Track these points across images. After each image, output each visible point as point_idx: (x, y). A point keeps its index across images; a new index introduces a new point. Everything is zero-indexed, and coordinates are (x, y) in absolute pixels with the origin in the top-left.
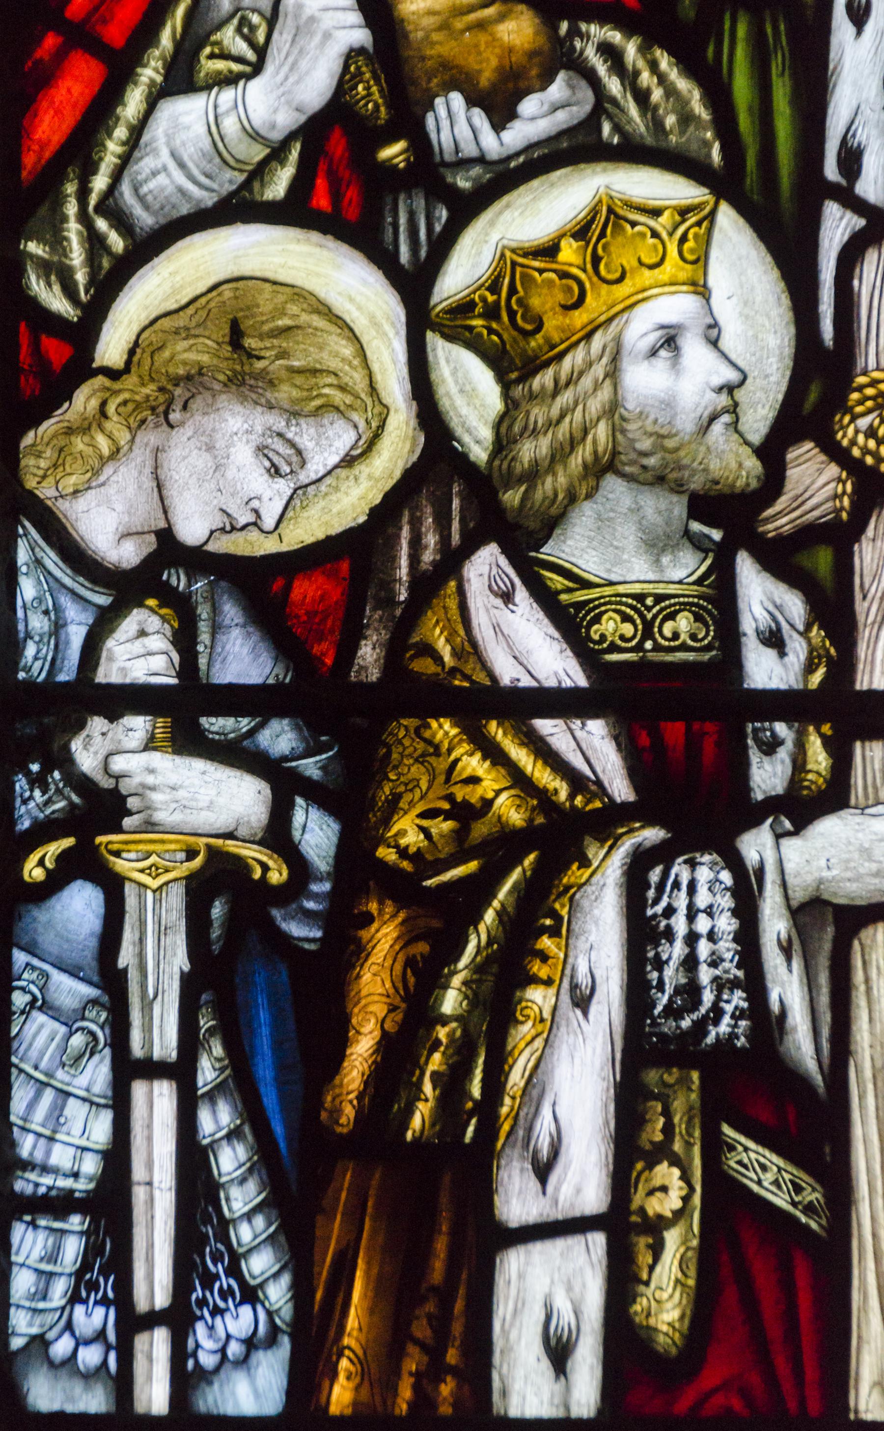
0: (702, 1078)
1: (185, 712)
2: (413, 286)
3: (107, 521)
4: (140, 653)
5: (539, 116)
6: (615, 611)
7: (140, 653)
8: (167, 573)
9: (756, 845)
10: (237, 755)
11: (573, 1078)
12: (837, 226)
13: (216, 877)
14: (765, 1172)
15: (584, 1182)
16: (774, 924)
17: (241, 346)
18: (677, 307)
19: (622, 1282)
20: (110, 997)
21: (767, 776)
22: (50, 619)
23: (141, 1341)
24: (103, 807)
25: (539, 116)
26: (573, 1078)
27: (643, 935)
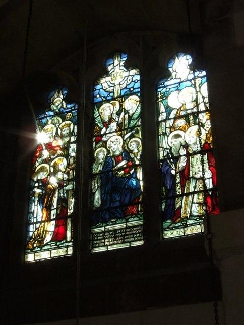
0: (20, 240)
1: (38, 188)
2: (50, 165)
3: (35, 179)
4: (36, 185)
5: (56, 156)
6: (131, 142)
7: (36, 185)
8: (38, 181)
9: (64, 188)
10: (40, 189)
11: (55, 200)
12: (69, 157)
13: (39, 195)
14: (64, 204)
15: (55, 207)
16: (65, 192)
17: (42, 169)
18: (62, 163)
19: (57, 211)
20: (29, 206)
21: (65, 185)
22: (199, 119)
23: (189, 82)
24: (34, 192)
25: (56, 156)
26: (55, 200)
27: (59, 193)
